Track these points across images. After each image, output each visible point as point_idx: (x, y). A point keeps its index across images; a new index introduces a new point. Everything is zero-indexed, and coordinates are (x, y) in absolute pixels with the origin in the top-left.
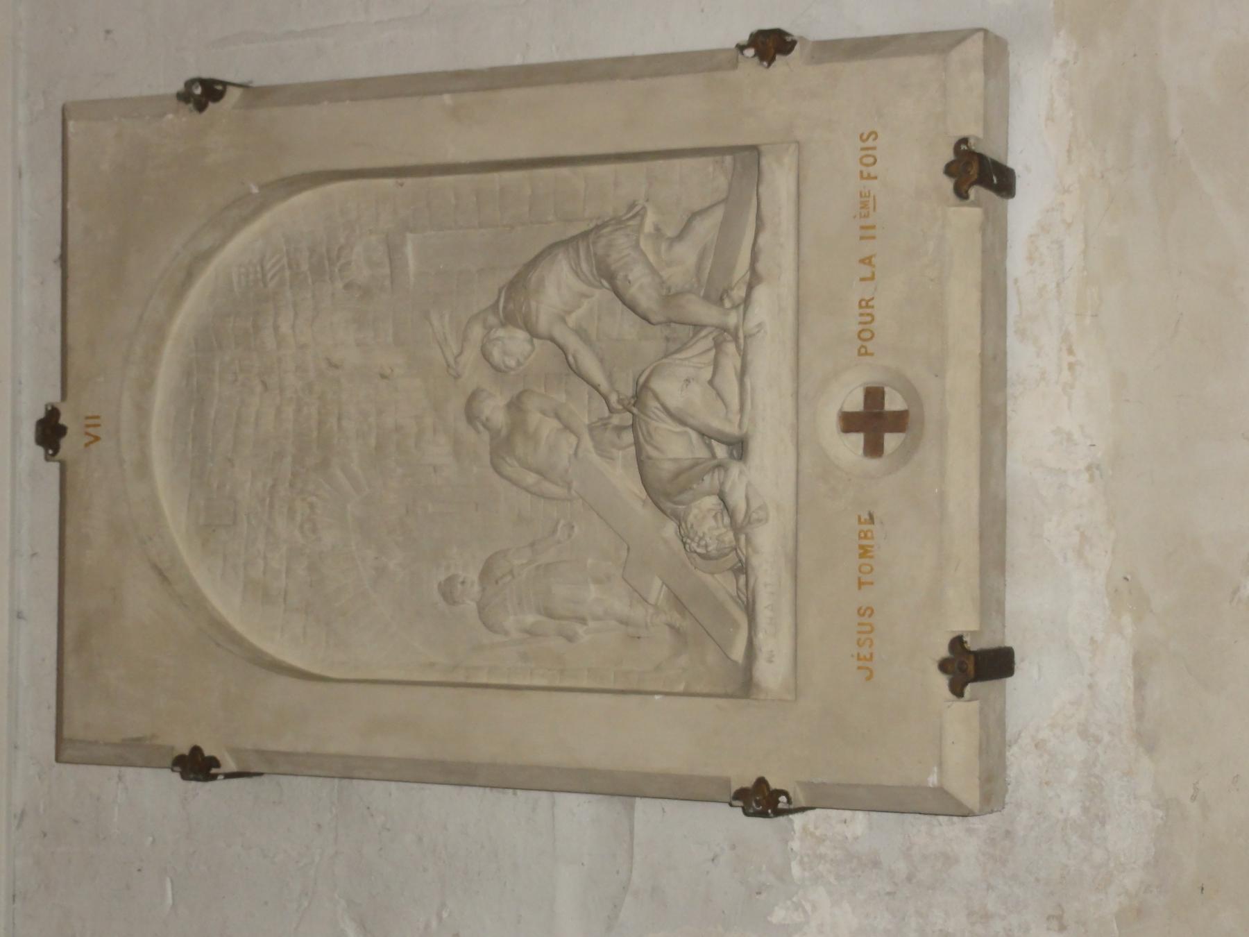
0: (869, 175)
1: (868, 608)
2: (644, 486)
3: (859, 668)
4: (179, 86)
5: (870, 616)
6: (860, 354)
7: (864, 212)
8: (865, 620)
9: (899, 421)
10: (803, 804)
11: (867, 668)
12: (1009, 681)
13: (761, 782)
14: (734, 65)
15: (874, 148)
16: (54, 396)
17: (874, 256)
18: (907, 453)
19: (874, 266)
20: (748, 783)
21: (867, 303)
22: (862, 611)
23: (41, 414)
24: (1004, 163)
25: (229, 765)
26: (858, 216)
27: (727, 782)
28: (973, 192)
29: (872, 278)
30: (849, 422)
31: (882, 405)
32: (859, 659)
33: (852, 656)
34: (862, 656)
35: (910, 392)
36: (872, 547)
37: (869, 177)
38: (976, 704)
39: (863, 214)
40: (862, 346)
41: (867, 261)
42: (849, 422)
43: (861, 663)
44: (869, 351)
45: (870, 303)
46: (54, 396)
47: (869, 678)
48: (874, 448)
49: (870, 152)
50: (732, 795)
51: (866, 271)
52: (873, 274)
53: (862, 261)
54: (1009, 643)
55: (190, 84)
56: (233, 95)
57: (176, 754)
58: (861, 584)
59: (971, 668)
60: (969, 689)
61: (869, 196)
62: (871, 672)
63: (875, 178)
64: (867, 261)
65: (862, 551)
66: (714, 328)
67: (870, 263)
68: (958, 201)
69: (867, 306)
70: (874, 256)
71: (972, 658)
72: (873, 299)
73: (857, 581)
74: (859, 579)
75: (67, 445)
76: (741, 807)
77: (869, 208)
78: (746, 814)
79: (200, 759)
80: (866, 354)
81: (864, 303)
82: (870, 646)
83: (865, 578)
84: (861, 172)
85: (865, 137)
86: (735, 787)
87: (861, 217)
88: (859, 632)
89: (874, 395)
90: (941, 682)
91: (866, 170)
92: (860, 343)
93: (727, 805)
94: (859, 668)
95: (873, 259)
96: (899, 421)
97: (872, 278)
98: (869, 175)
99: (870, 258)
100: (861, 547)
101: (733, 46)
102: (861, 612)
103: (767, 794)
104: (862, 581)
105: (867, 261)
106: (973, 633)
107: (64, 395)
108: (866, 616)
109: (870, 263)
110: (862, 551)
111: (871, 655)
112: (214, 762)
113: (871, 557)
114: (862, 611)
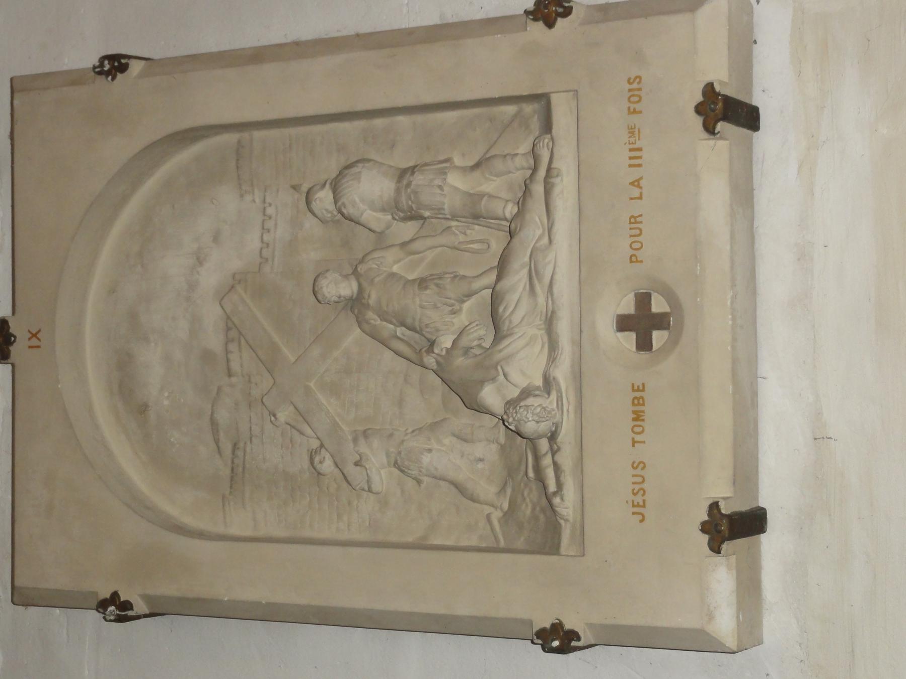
0: (634, 109)
2: (307, 203)
3: (634, 513)
5: (643, 468)
6: (631, 262)
7: (632, 140)
9: (661, 322)
10: (593, 642)
11: (638, 242)
12: (763, 537)
17: (641, 178)
18: (674, 342)
19: (641, 188)
24: (750, 103)
25: (140, 607)
26: (628, 143)
28: (720, 126)
29: (640, 198)
30: (624, 324)
31: (650, 309)
32: (633, 506)
34: (635, 503)
35: (670, 296)
36: (643, 412)
37: (635, 112)
38: (733, 559)
39: (631, 142)
40: (634, 255)
41: (636, 184)
42: (624, 324)
43: (636, 510)
44: (639, 259)
45: (638, 219)
47: (641, 521)
48: (644, 344)
49: (636, 93)
51: (636, 192)
52: (641, 194)
54: (762, 504)
56: (136, 67)
58: (634, 442)
59: (724, 527)
60: (725, 546)
61: (635, 127)
62: (643, 516)
63: (640, 112)
67: (639, 187)
68: (705, 135)
70: (641, 178)
72: (641, 216)
74: (633, 439)
77: (635, 137)
78: (545, 651)
80: (637, 261)
81: (633, 220)
82: (643, 495)
83: (638, 438)
84: (629, 108)
85: (631, 81)
86: (536, 628)
87: (629, 144)
88: (634, 483)
89: (643, 300)
91: (632, 106)
93: (530, 641)
94: (634, 513)
95: (640, 182)
96: (661, 322)
97: (640, 198)
98: (634, 109)
99: (638, 180)
100: (634, 412)
101: (522, 12)
103: (562, 633)
105: (636, 183)
106: (725, 499)
107: (14, 313)
109: (639, 187)
111: (644, 501)
112: (126, 606)
113: (643, 420)
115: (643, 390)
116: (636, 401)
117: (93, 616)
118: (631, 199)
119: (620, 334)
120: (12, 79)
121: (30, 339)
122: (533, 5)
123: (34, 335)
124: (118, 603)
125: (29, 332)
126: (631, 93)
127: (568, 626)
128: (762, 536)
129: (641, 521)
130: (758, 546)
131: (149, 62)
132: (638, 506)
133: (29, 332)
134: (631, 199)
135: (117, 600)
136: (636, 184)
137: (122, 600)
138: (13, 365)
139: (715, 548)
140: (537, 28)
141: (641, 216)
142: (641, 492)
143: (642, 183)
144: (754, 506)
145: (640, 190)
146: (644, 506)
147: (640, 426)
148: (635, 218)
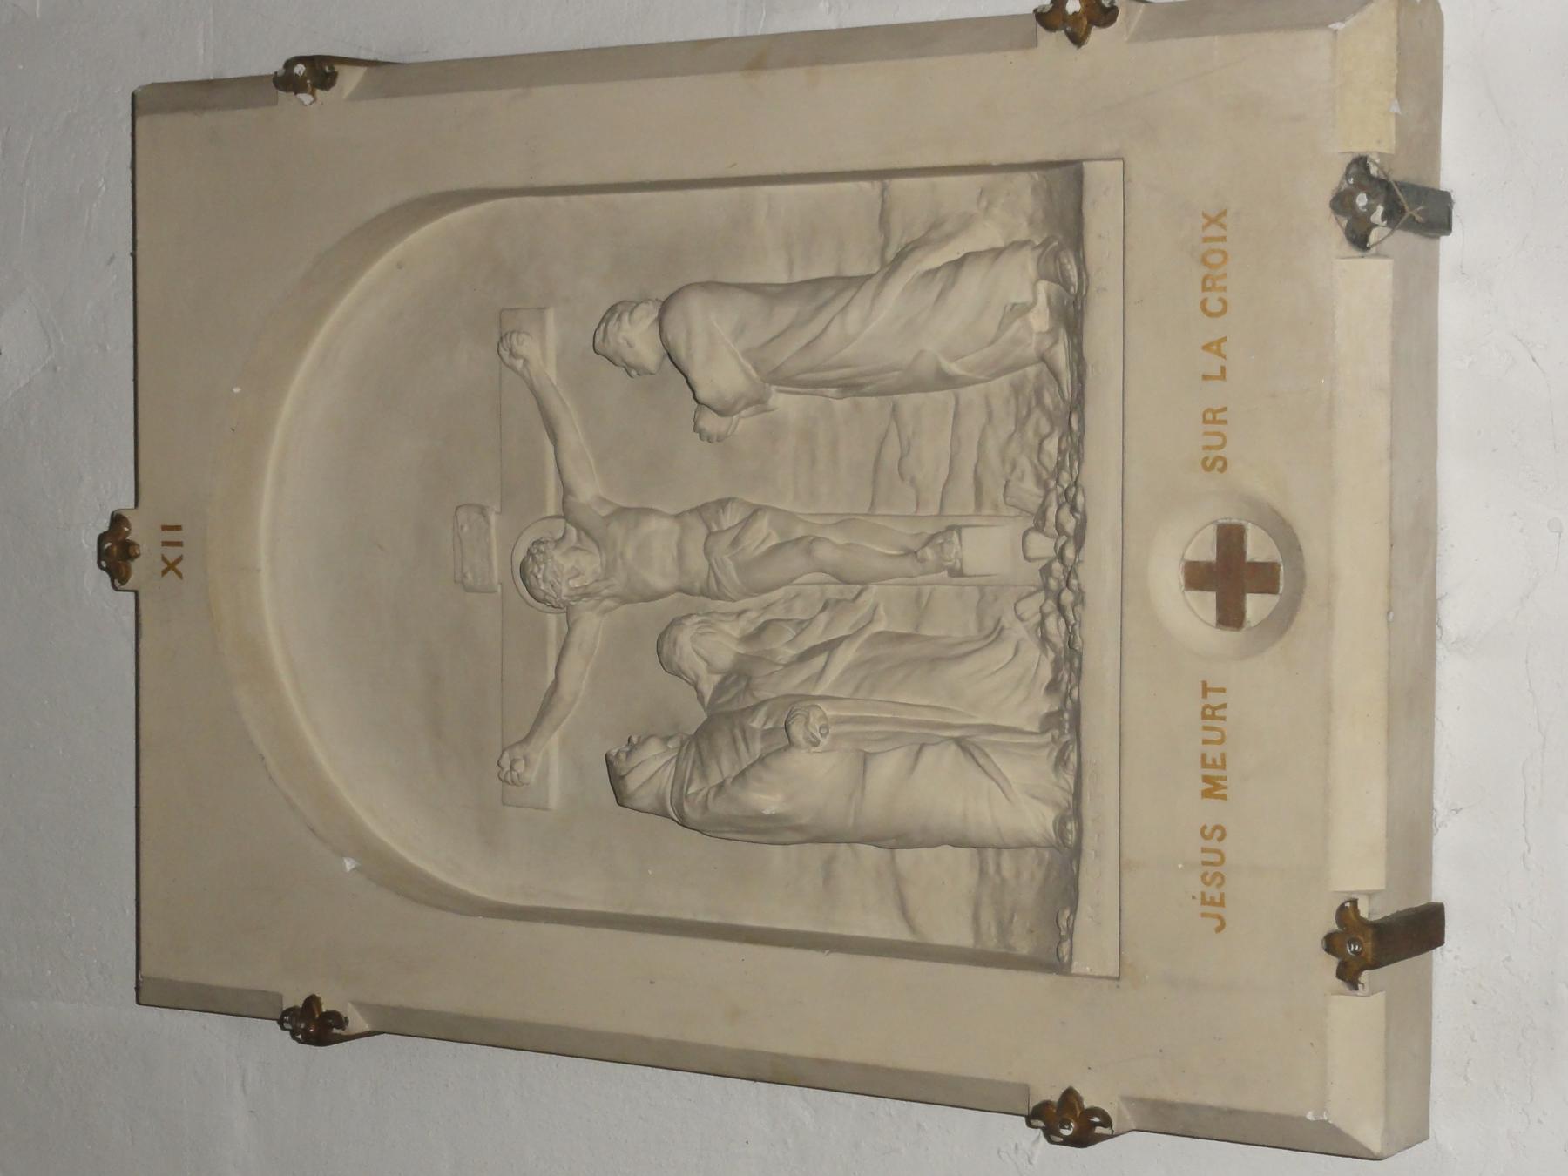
1: (1217, 827)
3: (1204, 915)
4: (277, 66)
5: (1221, 839)
8: (1213, 844)
9: (1265, 577)
13: (1070, 1096)
14: (1033, 43)
15: (1223, 239)
16: (125, 502)
17: (1224, 339)
18: (1281, 623)
20: (1054, 1096)
21: (1213, 713)
22: (1207, 832)
23: (104, 525)
25: (358, 1023)
27: (1025, 1089)
30: (1197, 577)
32: (1204, 902)
33: (1194, 897)
38: (1380, 998)
42: (1197, 577)
43: (1209, 723)
46: (125, 502)
47: (1219, 930)
48: (1230, 616)
50: (1031, 1106)
51: (1213, 364)
53: (1207, 347)
54: (1436, 898)
55: (290, 64)
56: (350, 79)
57: (284, 1009)
60: (1365, 977)
64: (1215, 347)
65: (1209, 786)
66: (1018, 511)
68: (1354, 252)
69: (1215, 421)
70: (1224, 339)
71: (1370, 933)
72: (1224, 409)
73: (1200, 688)
75: (139, 569)
76: (1042, 1128)
79: (317, 1016)
81: (1208, 712)
84: (1204, 757)
89: (1230, 538)
90: (1333, 231)
92: (1204, 271)
94: (1204, 915)
96: (1265, 577)
100: (1206, 779)
102: (1206, 690)
104: (1222, 344)
105: (1215, 347)
106: (1370, 895)
107: (136, 504)
108: (1215, 838)
110: (1209, 786)
111: (1222, 895)
112: (338, 1019)
114: (1207, 832)
115: (1223, 767)
116: (1209, 284)
117: (277, 1038)
118: (1205, 377)
119: (1193, 595)
120: (134, 96)
121: (180, 559)
122: (1049, 3)
123: (171, 566)
124: (317, 1016)
125: (179, 574)
126: (1207, 246)
127: (1090, 1099)
128: (1436, 952)
129: (1219, 930)
130: (1437, 249)
131: (373, 69)
132: (1212, 903)
133: (179, 574)
134: (1205, 377)
135: (316, 1012)
136: (1214, 347)
137: (324, 1011)
138: (136, 593)
139: (1349, 975)
140: (1053, 43)
141: (1224, 409)
142: (1218, 880)
143: (1224, 348)
144: (1419, 903)
145: (1220, 361)
146: (1222, 904)
147: (1218, 434)
148: (1215, 412)
